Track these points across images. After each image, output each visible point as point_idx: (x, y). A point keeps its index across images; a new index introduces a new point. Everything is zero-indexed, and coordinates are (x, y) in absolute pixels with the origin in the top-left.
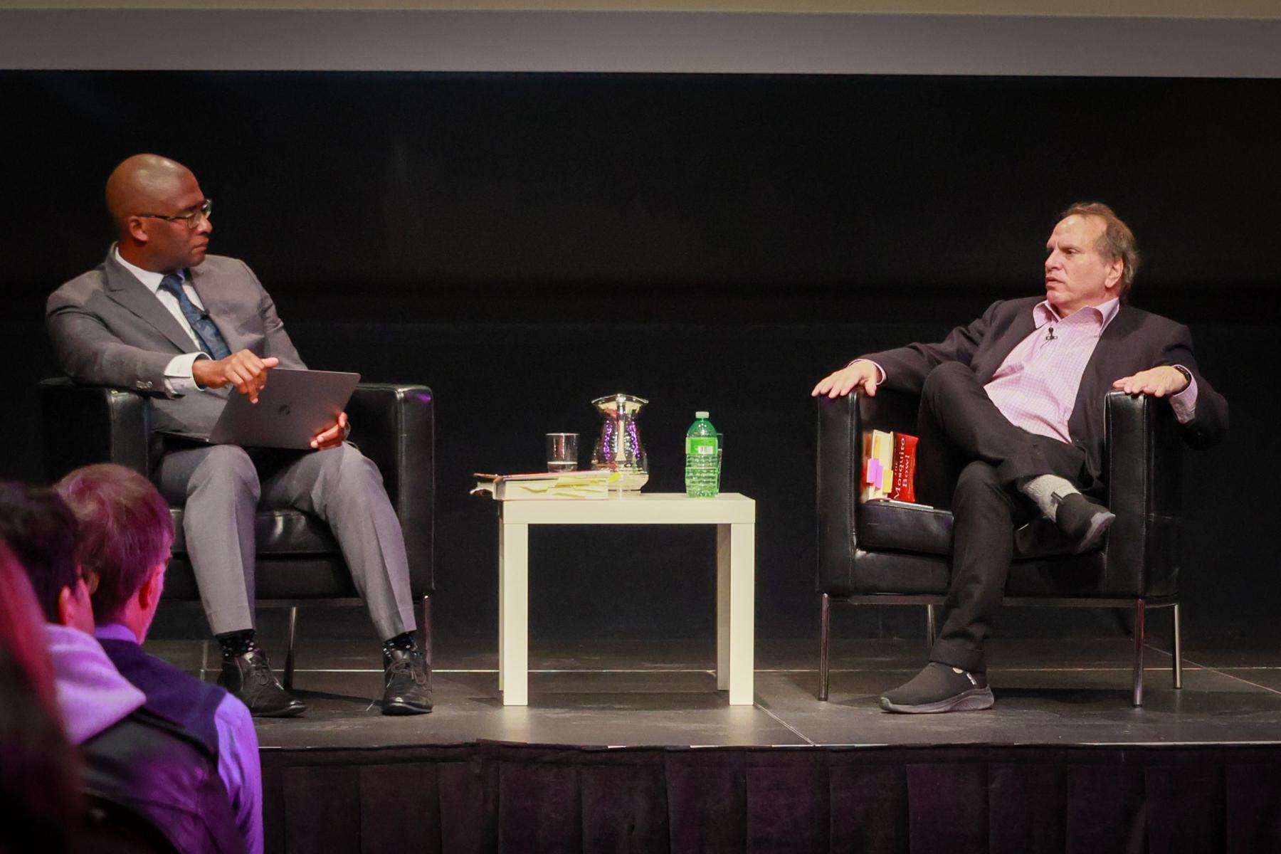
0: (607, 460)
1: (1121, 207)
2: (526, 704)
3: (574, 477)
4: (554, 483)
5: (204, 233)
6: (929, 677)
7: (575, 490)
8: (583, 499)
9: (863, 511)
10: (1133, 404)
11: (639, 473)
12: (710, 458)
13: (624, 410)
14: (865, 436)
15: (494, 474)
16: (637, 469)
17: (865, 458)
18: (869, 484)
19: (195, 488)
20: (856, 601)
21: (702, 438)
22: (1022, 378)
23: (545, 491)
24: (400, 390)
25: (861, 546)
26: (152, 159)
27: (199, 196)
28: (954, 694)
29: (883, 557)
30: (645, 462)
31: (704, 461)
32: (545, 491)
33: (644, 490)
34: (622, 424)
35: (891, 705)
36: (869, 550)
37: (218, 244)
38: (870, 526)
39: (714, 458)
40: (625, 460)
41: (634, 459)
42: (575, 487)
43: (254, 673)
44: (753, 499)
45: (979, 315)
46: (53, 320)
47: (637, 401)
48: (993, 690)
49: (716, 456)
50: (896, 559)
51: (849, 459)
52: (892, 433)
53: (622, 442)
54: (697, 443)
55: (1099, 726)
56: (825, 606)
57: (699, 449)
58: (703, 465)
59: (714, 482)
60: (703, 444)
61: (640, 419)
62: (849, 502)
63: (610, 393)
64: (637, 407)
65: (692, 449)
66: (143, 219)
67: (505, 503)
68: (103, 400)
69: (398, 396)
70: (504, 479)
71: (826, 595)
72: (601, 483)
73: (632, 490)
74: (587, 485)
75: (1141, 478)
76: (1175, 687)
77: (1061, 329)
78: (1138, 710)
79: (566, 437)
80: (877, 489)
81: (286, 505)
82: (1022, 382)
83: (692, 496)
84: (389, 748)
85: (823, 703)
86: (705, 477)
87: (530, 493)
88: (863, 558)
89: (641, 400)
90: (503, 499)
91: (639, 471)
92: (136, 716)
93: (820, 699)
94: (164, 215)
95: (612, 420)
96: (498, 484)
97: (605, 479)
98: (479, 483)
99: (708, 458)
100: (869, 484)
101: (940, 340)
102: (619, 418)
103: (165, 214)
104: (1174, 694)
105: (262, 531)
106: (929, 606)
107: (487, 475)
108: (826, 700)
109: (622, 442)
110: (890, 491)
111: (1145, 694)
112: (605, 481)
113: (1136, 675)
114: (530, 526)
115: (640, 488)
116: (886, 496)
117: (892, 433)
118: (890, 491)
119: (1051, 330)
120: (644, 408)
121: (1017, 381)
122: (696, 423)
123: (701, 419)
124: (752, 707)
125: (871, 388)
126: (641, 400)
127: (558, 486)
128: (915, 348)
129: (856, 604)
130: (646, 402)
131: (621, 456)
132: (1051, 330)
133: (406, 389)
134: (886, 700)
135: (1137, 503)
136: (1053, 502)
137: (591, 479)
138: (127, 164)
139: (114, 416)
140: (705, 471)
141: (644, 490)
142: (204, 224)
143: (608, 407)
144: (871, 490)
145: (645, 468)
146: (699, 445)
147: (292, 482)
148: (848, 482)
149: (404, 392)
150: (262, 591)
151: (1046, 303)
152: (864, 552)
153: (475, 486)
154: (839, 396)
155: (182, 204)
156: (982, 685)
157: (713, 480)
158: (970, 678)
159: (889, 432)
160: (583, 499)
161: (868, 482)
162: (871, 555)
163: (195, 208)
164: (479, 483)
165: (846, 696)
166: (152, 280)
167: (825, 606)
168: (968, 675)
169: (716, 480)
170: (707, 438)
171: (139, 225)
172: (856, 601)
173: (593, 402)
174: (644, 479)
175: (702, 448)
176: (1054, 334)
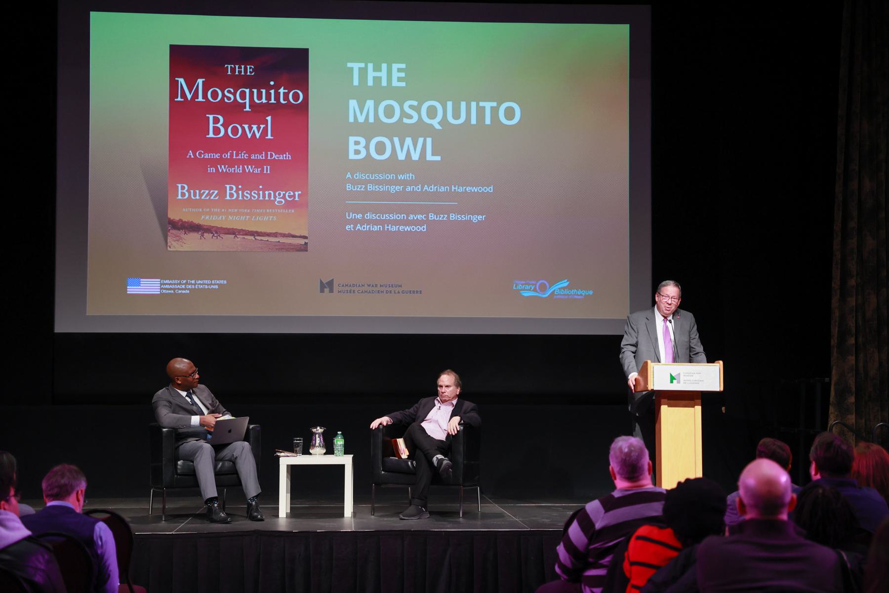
1: (455, 370)
2: (285, 516)
5: (197, 379)
6: (412, 509)
10: (10, 497)
15: (792, 464)
26: (179, 359)
27: (194, 368)
28: (419, 514)
29: (390, 474)
34: (317, 436)
35: (403, 518)
36: (386, 472)
37: (200, 381)
43: (217, 510)
45: (417, 402)
46: (661, 286)
53: (318, 440)
55: (534, 517)
56: (374, 488)
61: (324, 434)
64: (322, 430)
66: (179, 377)
68: (162, 432)
77: (443, 407)
78: (461, 520)
81: (222, 460)
83: (336, 456)
84: (229, 532)
92: (27, 539)
94: (185, 375)
101: (409, 409)
103: (185, 375)
104: (478, 513)
105: (215, 467)
108: (373, 515)
109: (318, 440)
111: (463, 513)
113: (460, 507)
119: (440, 407)
121: (431, 422)
132: (440, 407)
134: (401, 516)
135: (460, 459)
138: (172, 362)
139: (164, 435)
142: (197, 376)
143: (314, 430)
147: (226, 452)
150: (219, 485)
151: (438, 398)
154: (375, 428)
155: (190, 372)
156: (426, 511)
162: (386, 473)
163: (194, 372)
166: (184, 394)
167: (374, 488)
171: (178, 379)
172: (383, 486)
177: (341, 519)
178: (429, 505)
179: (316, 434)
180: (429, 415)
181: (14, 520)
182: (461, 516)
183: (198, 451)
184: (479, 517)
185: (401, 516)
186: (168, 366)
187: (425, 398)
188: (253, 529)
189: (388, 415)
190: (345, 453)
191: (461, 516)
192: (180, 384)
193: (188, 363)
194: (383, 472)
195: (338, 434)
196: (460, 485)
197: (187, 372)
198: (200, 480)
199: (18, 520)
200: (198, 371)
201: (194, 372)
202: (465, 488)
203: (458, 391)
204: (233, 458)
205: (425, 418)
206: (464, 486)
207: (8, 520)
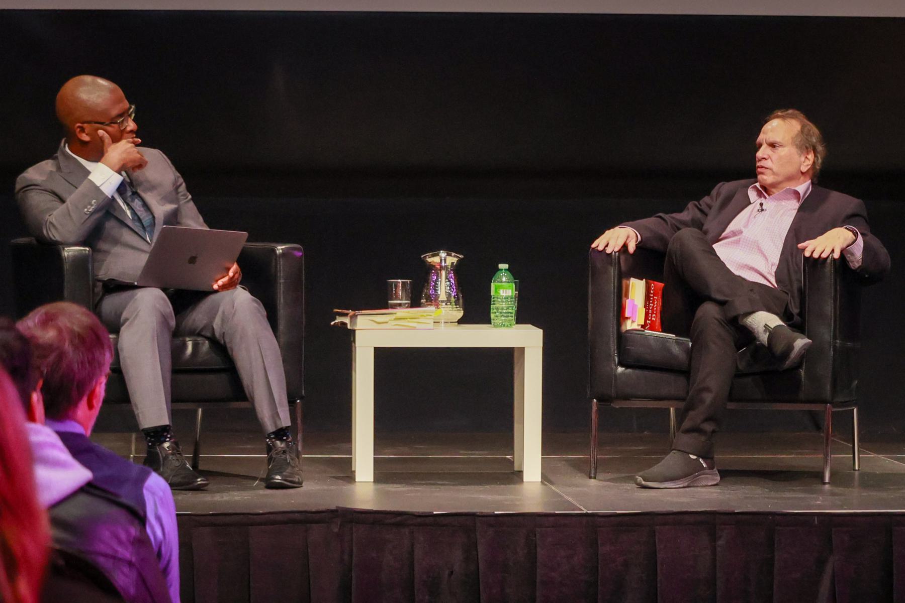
0: (433, 300)
2: (373, 481)
3: (408, 312)
4: (393, 317)
6: (671, 461)
7: (409, 322)
8: (414, 328)
9: (622, 338)
11: (455, 309)
12: (509, 298)
13: (445, 262)
14: (624, 282)
16: (455, 306)
17: (624, 299)
18: (627, 318)
19: (127, 320)
20: (617, 405)
21: (503, 284)
22: (741, 240)
23: (387, 322)
24: (279, 248)
25: (621, 364)
26: (88, 79)
27: (126, 104)
28: (690, 474)
30: (461, 301)
31: (504, 300)
32: (387, 322)
33: (460, 322)
35: (643, 483)
36: (627, 366)
38: (629, 349)
39: (511, 298)
40: (446, 299)
41: (453, 299)
42: (409, 319)
44: (541, 328)
45: (708, 193)
47: (455, 256)
48: (719, 471)
49: (513, 297)
50: (647, 373)
51: (612, 298)
52: (644, 280)
53: (444, 286)
54: (500, 287)
56: (594, 408)
57: (501, 292)
58: (504, 303)
59: (512, 317)
60: (504, 288)
61: (457, 270)
62: (612, 330)
63: (434, 249)
64: (455, 260)
65: (496, 291)
66: (85, 125)
67: (357, 331)
69: (278, 252)
70: (357, 314)
71: (595, 400)
72: (429, 317)
73: (451, 322)
74: (419, 318)
75: (830, 314)
76: (854, 470)
79: (402, 282)
80: (633, 322)
82: (741, 242)
83: (495, 326)
85: (593, 480)
86: (506, 313)
87: (375, 324)
88: (623, 374)
89: (458, 255)
90: (356, 329)
91: (457, 308)
93: (590, 478)
95: (436, 270)
96: (351, 318)
97: (431, 314)
98: (337, 317)
99: (508, 298)
100: (627, 318)
102: (441, 268)
105: (177, 351)
106: (672, 409)
107: (343, 311)
108: (595, 478)
109: (444, 286)
110: (643, 324)
112: (431, 315)
114: (376, 349)
115: (457, 321)
116: (640, 327)
117: (644, 280)
118: (643, 324)
119: (761, 205)
120: (460, 261)
121: (738, 242)
122: (499, 272)
123: (502, 270)
124: (540, 483)
125: (632, 248)
126: (458, 255)
127: (396, 319)
128: (660, 217)
129: (617, 407)
130: (461, 256)
131: (443, 296)
132: (761, 205)
133: (283, 247)
134: (640, 479)
136: (765, 331)
137: (421, 314)
139: (66, 267)
140: (505, 308)
141: (460, 322)
144: (629, 322)
145: (461, 307)
146: (502, 288)
147: (198, 316)
148: (611, 316)
149: (282, 249)
152: (624, 369)
153: (335, 319)
155: (115, 112)
156: (711, 467)
157: (512, 315)
158: (702, 462)
159: (642, 280)
160: (414, 328)
161: (626, 316)
162: (629, 371)
163: (124, 114)
164: (337, 317)
165: (609, 476)
167: (594, 408)
168: (700, 460)
169: (513, 315)
170: (507, 284)
171: (82, 130)
172: (617, 405)
173: (422, 257)
174: (460, 314)
175: (503, 291)
176: (764, 207)
177: (517, 486)
178: (717, 457)
179: (441, 268)
180: (729, 227)
181: (53, 446)
182: (827, 480)
183: (124, 308)
184: (856, 483)
185: (640, 479)
186: (58, 97)
187: (728, 181)
188: (333, 507)
189: (631, 223)
190: (519, 321)
191: (827, 480)
192: (86, 143)
193: (112, 91)
194: (620, 369)
195: (498, 270)
196: (827, 403)
197: (104, 112)
198: (126, 380)
199: (60, 443)
200: (137, 111)
201: (124, 114)
202: (835, 410)
203: (807, 162)
204: (409, 305)
205: (724, 230)
206: (834, 405)
207: (42, 445)
